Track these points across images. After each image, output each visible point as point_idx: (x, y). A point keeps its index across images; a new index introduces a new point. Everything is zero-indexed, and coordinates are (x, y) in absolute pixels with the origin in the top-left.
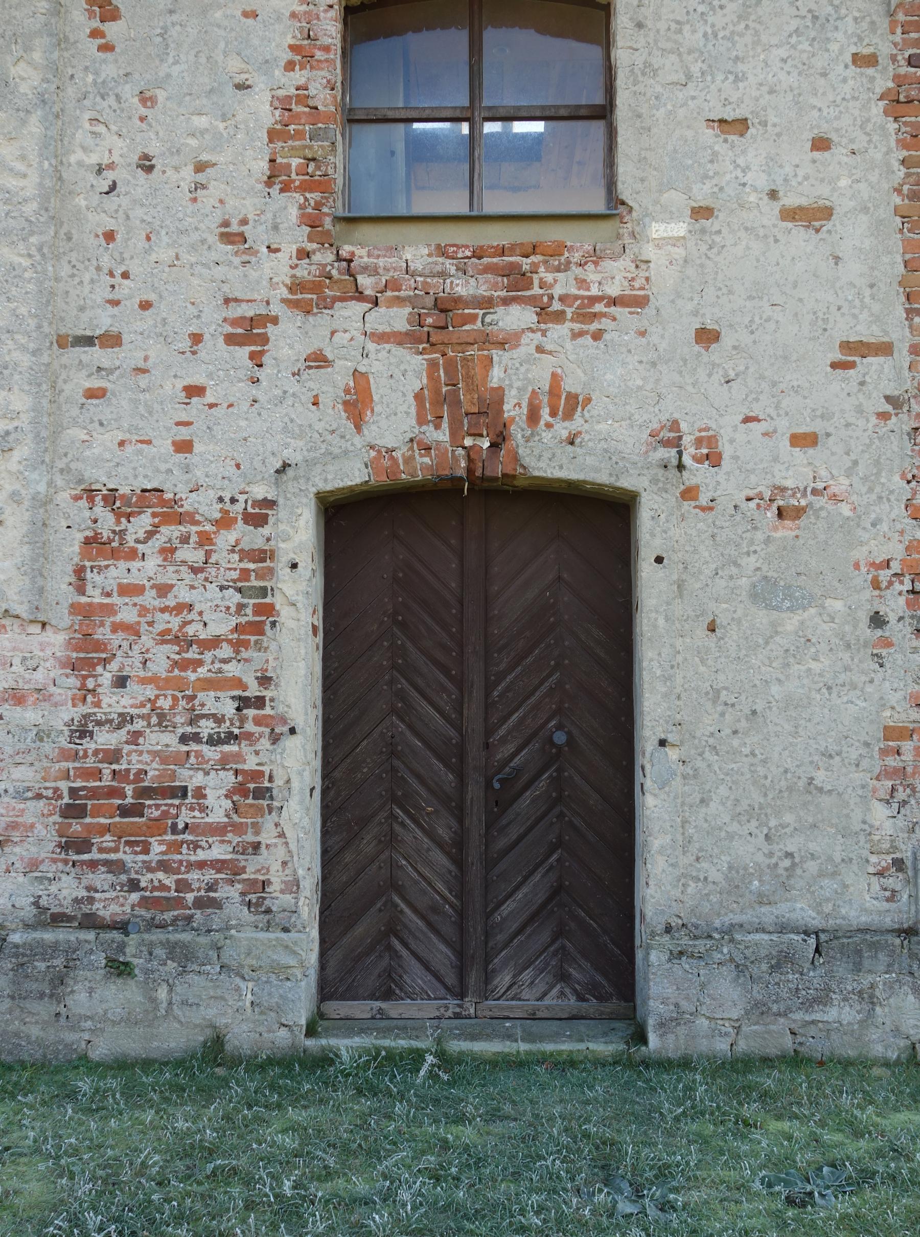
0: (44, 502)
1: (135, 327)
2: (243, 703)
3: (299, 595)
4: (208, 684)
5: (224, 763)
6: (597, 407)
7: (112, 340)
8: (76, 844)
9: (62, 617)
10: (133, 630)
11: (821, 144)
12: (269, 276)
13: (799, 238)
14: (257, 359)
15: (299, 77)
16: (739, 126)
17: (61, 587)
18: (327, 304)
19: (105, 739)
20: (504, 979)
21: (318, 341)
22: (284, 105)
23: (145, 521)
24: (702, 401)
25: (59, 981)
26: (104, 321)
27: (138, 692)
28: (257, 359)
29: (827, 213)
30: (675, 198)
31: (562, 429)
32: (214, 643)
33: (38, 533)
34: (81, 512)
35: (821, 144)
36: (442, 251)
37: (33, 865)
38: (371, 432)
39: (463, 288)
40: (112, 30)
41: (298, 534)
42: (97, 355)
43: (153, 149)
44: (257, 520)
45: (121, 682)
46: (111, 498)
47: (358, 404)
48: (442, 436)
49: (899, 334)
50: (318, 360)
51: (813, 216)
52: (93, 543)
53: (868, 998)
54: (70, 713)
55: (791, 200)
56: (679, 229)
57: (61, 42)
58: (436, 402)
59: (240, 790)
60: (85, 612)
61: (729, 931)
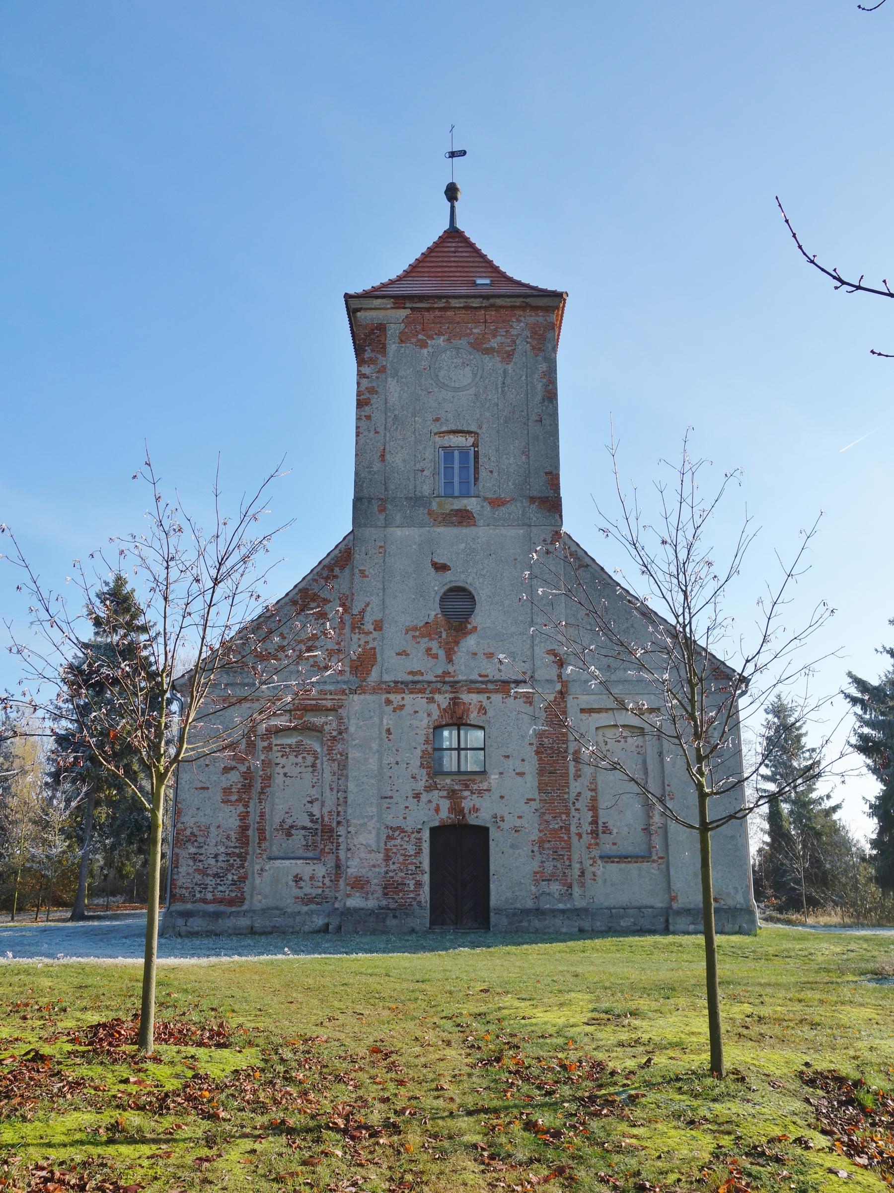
0: (379, 829)
1: (395, 794)
2: (416, 867)
3: (426, 846)
4: (410, 864)
5: (413, 879)
6: (482, 811)
7: (391, 797)
8: (385, 894)
9: (383, 851)
10: (396, 853)
11: (523, 760)
12: (421, 785)
13: (519, 779)
14: (418, 801)
15: (426, 746)
16: (508, 757)
17: (382, 845)
18: (431, 790)
19: (391, 874)
20: (465, 922)
21: (430, 798)
22: (423, 751)
23: (398, 833)
24: (501, 810)
25: (384, 920)
26: (390, 794)
27: (397, 865)
28: (418, 801)
29: (524, 774)
30: (496, 771)
31: (475, 815)
32: (411, 856)
33: (378, 836)
34: (386, 831)
35: (523, 760)
36: (453, 780)
37: (378, 898)
38: (440, 815)
39: (457, 787)
40: (391, 737)
41: (426, 835)
42: (388, 800)
43: (399, 760)
44: (419, 832)
45: (394, 863)
46: (391, 828)
47: (437, 810)
48: (453, 816)
49: (537, 797)
50: (430, 801)
51: (521, 774)
52: (388, 837)
53: (529, 921)
54: (384, 869)
55: (517, 771)
56: (497, 777)
57: (381, 739)
58: (451, 810)
59: (416, 884)
60: (387, 850)
61: (505, 910)
